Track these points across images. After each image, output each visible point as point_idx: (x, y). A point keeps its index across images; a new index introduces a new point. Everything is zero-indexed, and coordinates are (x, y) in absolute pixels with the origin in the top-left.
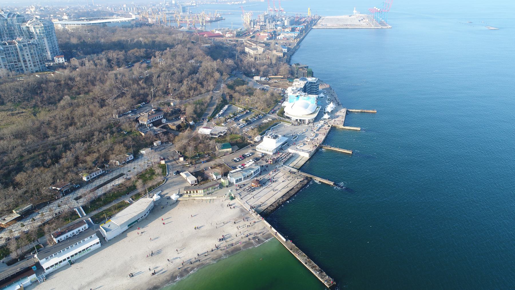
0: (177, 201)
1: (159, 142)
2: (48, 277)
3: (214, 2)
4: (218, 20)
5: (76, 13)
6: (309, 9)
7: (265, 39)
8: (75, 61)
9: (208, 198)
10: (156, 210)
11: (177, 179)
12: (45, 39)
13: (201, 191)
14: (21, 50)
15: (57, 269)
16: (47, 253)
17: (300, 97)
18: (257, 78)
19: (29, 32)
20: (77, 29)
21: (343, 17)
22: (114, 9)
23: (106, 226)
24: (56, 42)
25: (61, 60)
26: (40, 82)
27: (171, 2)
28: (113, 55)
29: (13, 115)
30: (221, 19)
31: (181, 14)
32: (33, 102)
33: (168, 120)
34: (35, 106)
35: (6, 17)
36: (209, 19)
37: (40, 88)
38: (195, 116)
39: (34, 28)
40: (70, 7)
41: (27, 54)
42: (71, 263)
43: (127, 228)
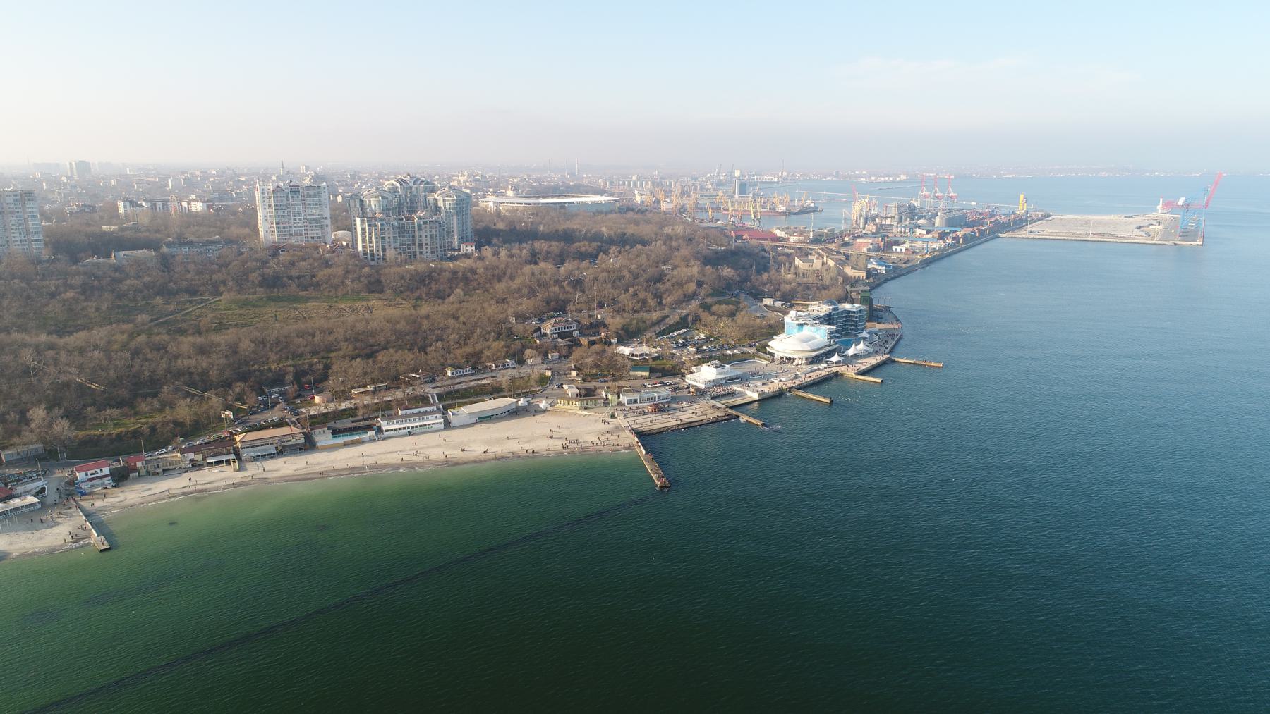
0: (546, 411)
1: (556, 355)
2: (385, 439)
3: (831, 175)
4: (806, 211)
5: (534, 187)
6: (1022, 197)
7: (865, 250)
8: (487, 251)
10: (515, 413)
12: (455, 218)
13: (578, 403)
14: (420, 228)
15: (396, 434)
16: (390, 417)
18: (768, 301)
20: (514, 211)
22: (611, 183)
25: (470, 249)
26: (432, 271)
28: (541, 245)
30: (815, 210)
31: (737, 196)
32: (417, 294)
33: (582, 334)
34: (417, 299)
38: (622, 332)
39: (444, 201)
40: (529, 176)
42: (410, 433)
43: (474, 420)
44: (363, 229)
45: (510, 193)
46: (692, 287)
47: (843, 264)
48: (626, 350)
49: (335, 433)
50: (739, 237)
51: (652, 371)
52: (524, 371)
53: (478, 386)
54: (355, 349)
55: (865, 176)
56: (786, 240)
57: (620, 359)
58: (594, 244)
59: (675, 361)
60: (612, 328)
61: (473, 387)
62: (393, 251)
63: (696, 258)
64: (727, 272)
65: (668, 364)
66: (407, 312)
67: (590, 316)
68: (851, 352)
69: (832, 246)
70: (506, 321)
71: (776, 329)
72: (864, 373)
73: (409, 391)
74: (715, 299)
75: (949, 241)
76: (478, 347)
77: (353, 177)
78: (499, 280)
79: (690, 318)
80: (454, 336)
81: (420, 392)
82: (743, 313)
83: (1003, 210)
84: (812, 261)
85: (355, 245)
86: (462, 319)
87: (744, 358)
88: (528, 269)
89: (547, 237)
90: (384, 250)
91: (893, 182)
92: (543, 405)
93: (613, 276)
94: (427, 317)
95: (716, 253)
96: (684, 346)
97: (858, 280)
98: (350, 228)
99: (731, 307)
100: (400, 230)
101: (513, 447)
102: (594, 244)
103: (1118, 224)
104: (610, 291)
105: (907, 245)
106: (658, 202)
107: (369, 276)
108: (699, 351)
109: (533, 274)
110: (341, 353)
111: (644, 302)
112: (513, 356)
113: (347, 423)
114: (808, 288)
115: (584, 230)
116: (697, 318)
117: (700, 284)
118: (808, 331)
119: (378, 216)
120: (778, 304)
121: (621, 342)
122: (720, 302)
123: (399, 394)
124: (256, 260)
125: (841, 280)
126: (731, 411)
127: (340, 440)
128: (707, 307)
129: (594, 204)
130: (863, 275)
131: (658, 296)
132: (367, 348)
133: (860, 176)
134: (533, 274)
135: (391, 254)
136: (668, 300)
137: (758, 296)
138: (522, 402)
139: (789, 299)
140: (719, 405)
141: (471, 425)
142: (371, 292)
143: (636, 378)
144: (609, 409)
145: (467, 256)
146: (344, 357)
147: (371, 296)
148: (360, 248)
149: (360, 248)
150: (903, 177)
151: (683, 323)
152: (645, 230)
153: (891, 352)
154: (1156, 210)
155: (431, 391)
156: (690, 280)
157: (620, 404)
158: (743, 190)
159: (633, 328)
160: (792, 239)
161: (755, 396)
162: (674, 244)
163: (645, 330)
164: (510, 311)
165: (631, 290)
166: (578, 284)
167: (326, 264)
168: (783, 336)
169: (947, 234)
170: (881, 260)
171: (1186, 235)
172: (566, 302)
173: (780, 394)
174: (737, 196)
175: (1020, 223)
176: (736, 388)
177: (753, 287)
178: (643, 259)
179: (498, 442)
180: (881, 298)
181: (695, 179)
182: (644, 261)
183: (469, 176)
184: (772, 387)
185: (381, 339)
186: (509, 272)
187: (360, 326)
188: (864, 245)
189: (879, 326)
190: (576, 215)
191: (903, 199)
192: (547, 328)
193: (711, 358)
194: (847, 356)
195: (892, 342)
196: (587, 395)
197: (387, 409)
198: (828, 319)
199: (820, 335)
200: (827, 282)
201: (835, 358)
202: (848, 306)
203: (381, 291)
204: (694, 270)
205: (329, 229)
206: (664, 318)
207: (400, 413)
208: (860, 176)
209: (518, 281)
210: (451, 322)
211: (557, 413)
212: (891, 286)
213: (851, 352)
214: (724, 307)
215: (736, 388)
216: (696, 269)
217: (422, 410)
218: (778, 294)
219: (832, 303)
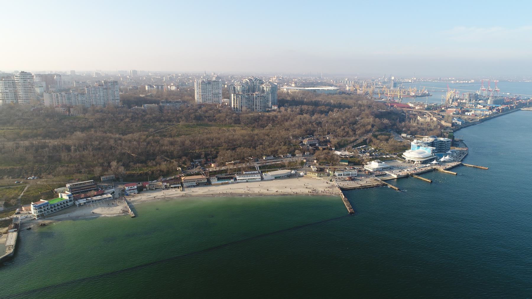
0: (303, 176)
1: (308, 153)
4: (424, 95)
7: (451, 114)
8: (282, 109)
9: (319, 178)
10: (290, 176)
11: (309, 168)
13: (317, 174)
14: (256, 99)
15: (242, 181)
16: (240, 174)
17: (421, 147)
18: (404, 135)
19: (263, 89)
22: (336, 82)
25: (276, 108)
26: (260, 116)
30: (428, 95)
33: (320, 145)
34: (254, 127)
36: (414, 94)
37: (259, 118)
39: (266, 88)
42: (247, 182)
44: (234, 99)
45: (293, 85)
46: (369, 127)
47: (441, 120)
48: (339, 153)
50: (392, 106)
51: (349, 162)
52: (294, 159)
53: (276, 164)
57: (335, 156)
58: (327, 107)
59: (360, 159)
62: (245, 108)
64: (386, 121)
65: (357, 160)
66: (249, 132)
67: (324, 138)
69: (436, 112)
70: (288, 138)
72: (445, 170)
73: (248, 164)
74: (379, 133)
75: (495, 111)
76: (277, 148)
78: (287, 121)
79: (368, 141)
80: (267, 143)
84: (426, 118)
86: (271, 136)
87: (391, 159)
88: (299, 117)
89: (307, 104)
90: (242, 107)
92: (302, 174)
93: (335, 121)
95: (381, 113)
96: (364, 152)
97: (447, 127)
98: (229, 98)
99: (387, 137)
100: (248, 99)
101: (288, 191)
102: (327, 107)
104: (333, 127)
105: (473, 112)
106: (356, 90)
108: (371, 155)
109: (301, 119)
111: (348, 133)
112: (290, 153)
113: (223, 176)
114: (423, 130)
117: (373, 126)
118: (422, 149)
121: (336, 149)
122: (382, 134)
125: (439, 127)
126: (384, 182)
127: (220, 182)
128: (375, 136)
129: (328, 90)
130: (450, 125)
131: (354, 131)
134: (301, 119)
135: (244, 109)
136: (358, 132)
137: (399, 132)
139: (414, 134)
141: (272, 180)
142: (235, 123)
144: (330, 178)
145: (274, 110)
148: (232, 106)
149: (232, 106)
150: (473, 81)
151: (364, 142)
152: (350, 102)
153: (462, 161)
155: (256, 165)
156: (369, 124)
157: (334, 175)
158: (395, 85)
159: (342, 144)
160: (417, 108)
161: (396, 176)
162: (362, 108)
163: (347, 144)
164: (291, 134)
165: (342, 127)
166: (319, 124)
167: (219, 112)
168: (410, 150)
169: (493, 108)
173: (407, 176)
174: (392, 88)
176: (387, 172)
177: (398, 128)
178: (348, 114)
180: (458, 136)
181: (373, 80)
183: (277, 78)
187: (231, 137)
188: (451, 112)
192: (305, 142)
193: (376, 159)
195: (463, 156)
196: (320, 171)
197: (239, 171)
198: (432, 144)
199: (428, 151)
200: (432, 128)
201: (434, 162)
202: (442, 139)
203: (240, 124)
204: (371, 120)
205: (221, 98)
210: (266, 137)
211: (307, 177)
212: (463, 130)
214: (383, 136)
215: (387, 172)
217: (253, 172)
218: (409, 132)
219: (434, 137)
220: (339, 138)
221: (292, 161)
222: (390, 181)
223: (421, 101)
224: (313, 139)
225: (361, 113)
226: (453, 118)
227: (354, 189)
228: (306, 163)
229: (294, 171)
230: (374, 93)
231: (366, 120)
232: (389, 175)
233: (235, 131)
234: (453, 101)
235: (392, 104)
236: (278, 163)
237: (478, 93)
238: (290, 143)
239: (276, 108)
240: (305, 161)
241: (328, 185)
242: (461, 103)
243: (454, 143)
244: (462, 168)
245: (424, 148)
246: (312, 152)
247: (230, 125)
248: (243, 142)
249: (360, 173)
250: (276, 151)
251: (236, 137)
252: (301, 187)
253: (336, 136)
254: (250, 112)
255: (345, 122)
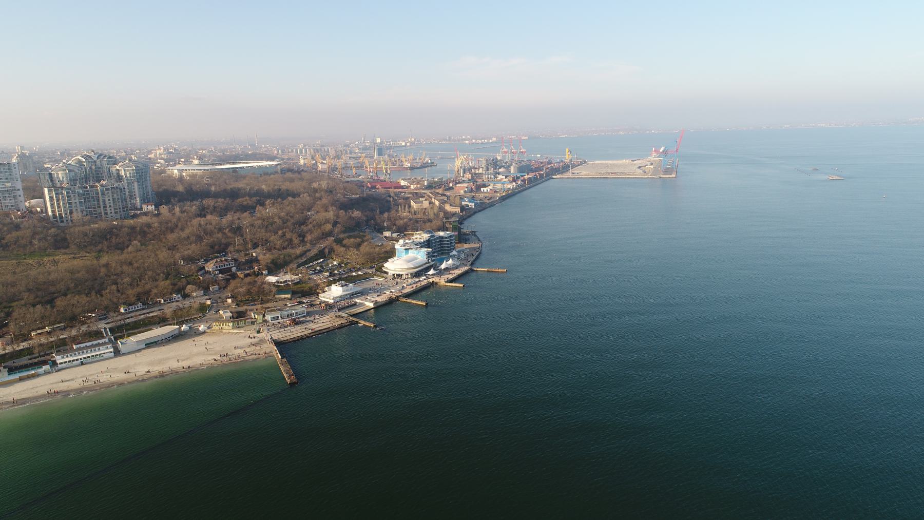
0: (204, 332)
1: (216, 287)
2: (59, 370)
4: (425, 166)
7: (462, 192)
8: (164, 209)
9: (236, 331)
11: (216, 316)
12: (136, 184)
13: (231, 324)
14: (103, 194)
15: (69, 366)
20: (193, 176)
21: (624, 161)
23: (123, 341)
24: (149, 188)
26: (116, 227)
27: (374, 140)
29: (74, 258)
30: (431, 165)
33: (239, 269)
34: (100, 251)
35: (95, 159)
39: (124, 170)
41: (108, 200)
42: (82, 364)
44: (51, 198)
45: (196, 162)
46: (328, 227)
47: (444, 202)
48: (272, 279)
49: (11, 371)
50: (374, 187)
51: (294, 293)
52: (187, 302)
53: (147, 318)
54: (37, 297)
55: (468, 140)
56: (408, 187)
57: (265, 286)
58: (254, 199)
59: (312, 285)
60: (263, 263)
61: (142, 320)
62: (80, 214)
63: (332, 205)
64: (356, 214)
65: (306, 287)
66: (89, 263)
67: (246, 255)
68: (443, 266)
69: (440, 191)
70: (175, 264)
71: (390, 254)
72: (447, 282)
73: (84, 328)
74: (346, 235)
75: (519, 183)
76: (148, 287)
77: (62, 154)
78: (172, 231)
79: (327, 250)
80: (127, 280)
81: (94, 328)
82: (365, 244)
83: (556, 158)
84: (422, 202)
85: (47, 212)
86: (136, 265)
87: (366, 277)
88: (196, 221)
89: (216, 195)
90: (71, 212)
91: (488, 143)
92: (202, 328)
93: (265, 223)
94: (107, 265)
95: (351, 200)
96: (320, 272)
97: (454, 214)
98: (42, 196)
99: (358, 240)
100: (85, 196)
101: (174, 365)
102: (254, 199)
103: (626, 166)
104: (262, 234)
105: (491, 187)
106: (316, 164)
107: (56, 235)
108: (331, 275)
109: (200, 225)
110: (23, 302)
111: (291, 241)
112: (178, 291)
113: (24, 361)
114: (417, 222)
115: (248, 188)
116: (331, 250)
117: (335, 224)
118: (412, 253)
119: (65, 185)
120: (395, 235)
121: (271, 273)
122: (349, 237)
123: (74, 332)
124: (367, 241)
125: (442, 215)
126: (352, 318)
127: (16, 376)
128: (339, 242)
129: (259, 167)
130: (458, 210)
131: (302, 236)
132: (46, 295)
133: (465, 140)
134: (200, 225)
135: (77, 216)
136: (309, 237)
137: (380, 230)
138: (184, 327)
139: (403, 231)
140: (343, 315)
141: (139, 350)
142: (57, 248)
143: (280, 300)
144: (256, 327)
145: (146, 214)
146: (25, 305)
147: (58, 252)
148: (50, 213)
149: (50, 213)
150: (494, 139)
151: (321, 254)
152: (296, 186)
153: (472, 264)
154: (651, 155)
155: (102, 326)
156: (327, 221)
157: (265, 321)
158: (380, 153)
159: (280, 261)
160: (413, 187)
161: (371, 305)
162: (317, 195)
163: (291, 261)
164: (178, 255)
165: (280, 232)
166: (238, 230)
167: (17, 227)
168: (395, 258)
169: (518, 178)
170: (473, 198)
171: (667, 171)
172: (227, 245)
173: (391, 302)
174: (376, 157)
175: (566, 168)
176: (358, 301)
177: (376, 224)
178: (291, 209)
179: (160, 362)
180: (466, 228)
181: (347, 146)
182: (293, 210)
183: (164, 150)
184: (382, 299)
185: (61, 287)
186: (180, 225)
187: (41, 278)
188: (461, 189)
189: (466, 246)
190: (244, 177)
191: (491, 156)
192: (210, 267)
193: (340, 280)
194: (441, 270)
195: (476, 257)
196: (239, 317)
197: (62, 346)
198: (427, 244)
199: (421, 256)
200: (432, 216)
201: (432, 272)
202: (442, 234)
203: (67, 247)
204: (331, 214)
205: (22, 198)
206: (306, 252)
207: (75, 347)
208: (465, 140)
209: (187, 231)
210: (125, 268)
211: (213, 333)
212: (479, 217)
213: (443, 266)
214: (352, 240)
215: (358, 301)
216: (332, 213)
217: (95, 342)
218: (394, 228)
219: (429, 232)
220: (274, 251)
221: (181, 306)
222: (362, 315)
223: (418, 175)
224: (227, 261)
225: (314, 203)
226: (462, 198)
227: (301, 339)
228: (210, 307)
229: (186, 324)
230: (346, 167)
231: (323, 215)
232: (361, 304)
233: (55, 263)
234: (464, 173)
235: (375, 181)
236: (152, 314)
237: (499, 158)
238: (178, 274)
239: (151, 208)
240: (209, 302)
241: (253, 341)
242: (475, 174)
243: (462, 238)
244: (473, 276)
245: (416, 252)
246: (223, 284)
247: (43, 252)
248: (73, 285)
249: (311, 309)
250: (148, 293)
251: (53, 277)
252: (198, 354)
253: (270, 250)
254: (90, 222)
255: (285, 222)
